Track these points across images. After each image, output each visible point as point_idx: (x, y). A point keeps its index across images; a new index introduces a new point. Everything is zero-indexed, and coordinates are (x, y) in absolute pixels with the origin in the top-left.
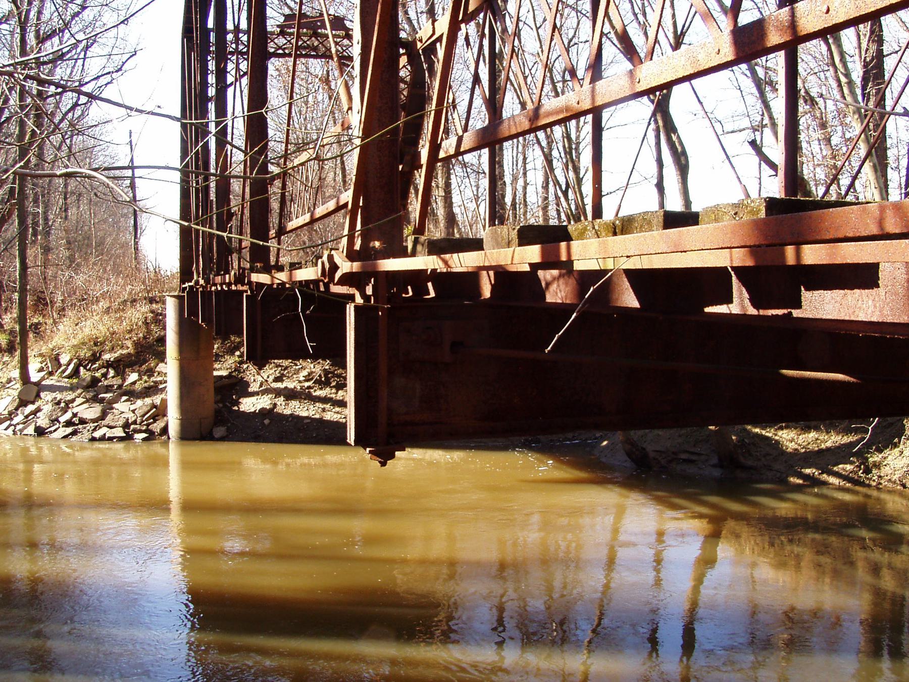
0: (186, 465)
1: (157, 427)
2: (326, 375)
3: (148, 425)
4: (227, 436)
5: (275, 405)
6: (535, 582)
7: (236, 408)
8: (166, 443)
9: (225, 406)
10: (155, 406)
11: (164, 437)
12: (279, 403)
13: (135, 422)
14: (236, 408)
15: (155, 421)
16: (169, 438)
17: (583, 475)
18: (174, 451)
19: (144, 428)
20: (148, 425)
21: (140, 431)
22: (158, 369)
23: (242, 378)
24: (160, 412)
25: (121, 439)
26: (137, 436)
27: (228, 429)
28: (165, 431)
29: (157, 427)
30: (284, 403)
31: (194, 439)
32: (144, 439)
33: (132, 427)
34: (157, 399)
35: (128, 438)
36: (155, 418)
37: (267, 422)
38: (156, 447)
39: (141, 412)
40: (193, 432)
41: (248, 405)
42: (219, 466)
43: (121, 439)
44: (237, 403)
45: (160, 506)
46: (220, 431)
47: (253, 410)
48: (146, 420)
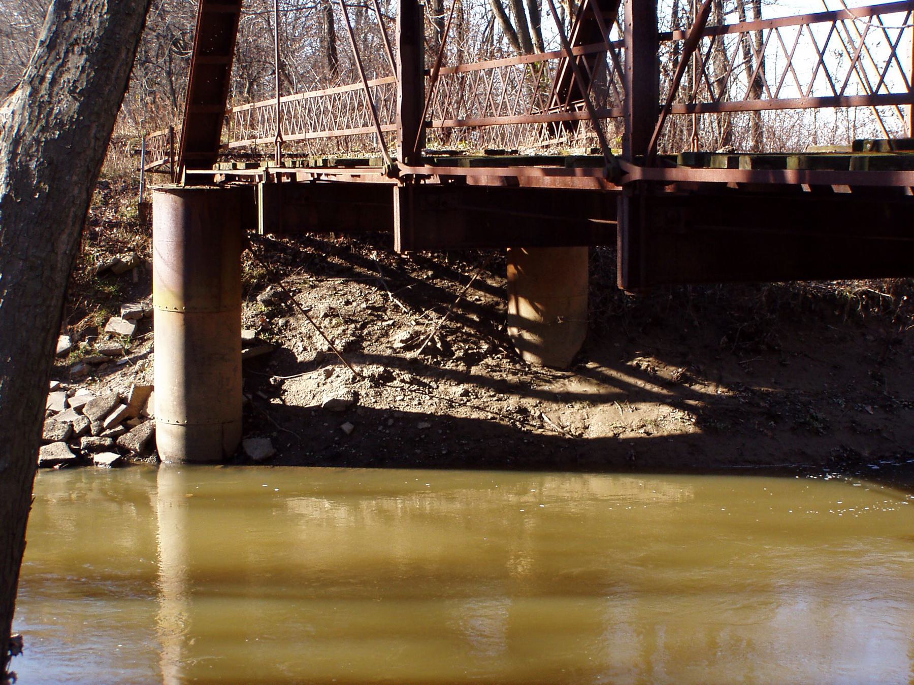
0: (193, 503)
1: (132, 440)
2: (442, 338)
3: (115, 436)
4: (275, 455)
5: (356, 395)
6: (804, 167)
7: (277, 401)
8: (152, 473)
9: (256, 398)
10: (121, 400)
11: (151, 459)
12: (363, 392)
13: (87, 431)
14: (277, 401)
15: (127, 429)
16: (159, 460)
17: (910, 84)
18: (167, 486)
19: (108, 441)
20: (115, 436)
21: (102, 449)
22: (108, 328)
23: (279, 345)
24: (135, 410)
25: (67, 464)
26: (97, 457)
27: (274, 441)
28: (150, 446)
29: (132, 440)
30: (372, 392)
31: (211, 462)
32: (114, 464)
33: (84, 440)
34: (119, 384)
35: (81, 461)
36: (126, 421)
37: (347, 427)
38: (132, 477)
39: (97, 412)
40: (207, 446)
41: (304, 391)
42: (257, 503)
43: (67, 464)
44: (278, 391)
45: (143, 585)
46: (259, 446)
47: (313, 403)
48: (110, 426)
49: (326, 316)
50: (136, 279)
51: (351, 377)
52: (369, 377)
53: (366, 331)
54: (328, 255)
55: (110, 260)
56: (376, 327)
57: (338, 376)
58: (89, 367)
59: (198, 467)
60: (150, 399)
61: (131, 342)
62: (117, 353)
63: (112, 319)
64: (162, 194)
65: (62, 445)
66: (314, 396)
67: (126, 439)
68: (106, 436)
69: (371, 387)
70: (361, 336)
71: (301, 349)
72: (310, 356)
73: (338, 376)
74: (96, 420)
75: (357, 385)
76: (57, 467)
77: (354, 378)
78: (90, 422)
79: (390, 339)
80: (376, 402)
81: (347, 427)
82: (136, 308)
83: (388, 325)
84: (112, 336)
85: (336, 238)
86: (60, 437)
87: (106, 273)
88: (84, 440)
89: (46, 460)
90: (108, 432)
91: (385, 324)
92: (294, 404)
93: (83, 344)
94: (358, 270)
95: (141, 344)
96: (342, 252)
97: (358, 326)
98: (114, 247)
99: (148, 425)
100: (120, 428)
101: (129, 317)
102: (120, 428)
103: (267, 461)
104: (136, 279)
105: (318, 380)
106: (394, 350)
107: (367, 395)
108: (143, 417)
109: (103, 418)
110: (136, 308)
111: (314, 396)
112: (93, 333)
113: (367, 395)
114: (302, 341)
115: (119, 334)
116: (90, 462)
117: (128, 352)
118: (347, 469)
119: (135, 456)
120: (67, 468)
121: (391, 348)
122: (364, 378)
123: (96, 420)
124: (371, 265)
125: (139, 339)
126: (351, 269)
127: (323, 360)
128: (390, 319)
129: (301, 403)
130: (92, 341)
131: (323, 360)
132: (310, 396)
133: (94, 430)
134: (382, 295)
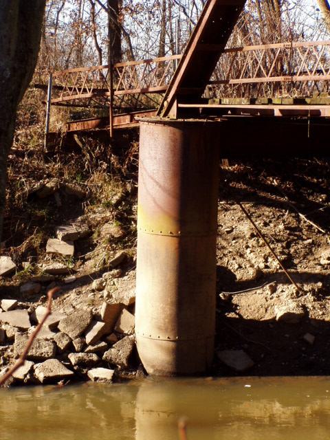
1: (118, 353)
3: (99, 352)
5: (304, 307)
12: (309, 306)
14: (232, 315)
15: (110, 346)
29: (118, 353)
46: (237, 358)
47: (268, 317)
49: (252, 236)
50: (59, 203)
51: (295, 292)
52: (310, 291)
53: (292, 250)
54: (230, 181)
55: (37, 185)
56: (299, 246)
57: (282, 291)
58: (39, 285)
59: (194, 380)
60: (122, 316)
61: (74, 262)
62: (65, 272)
63: (50, 241)
64: (152, 126)
65: (55, 362)
66: (266, 310)
67: (110, 354)
68: (90, 351)
69: (314, 300)
70: (289, 254)
71: (237, 266)
72: (250, 273)
73: (282, 291)
74: (76, 337)
75: (302, 299)
76: (60, 383)
77: (297, 293)
78: (71, 340)
79: (316, 257)
80: (323, 314)
81: (309, 338)
82: (72, 229)
83: (309, 244)
84: (55, 256)
85: (230, 165)
86: (50, 355)
87: (34, 196)
88: (73, 358)
89: (49, 377)
90: (90, 348)
91: (306, 242)
92: (251, 317)
93: (26, 265)
94: (262, 194)
95: (83, 263)
96: (239, 177)
97: (284, 244)
98: (36, 174)
99: (128, 341)
100: (103, 344)
101: (67, 239)
102: (103, 344)
103: (248, 372)
104: (59, 203)
105: (264, 295)
106: (323, 266)
107: (314, 308)
108: (121, 335)
109: (82, 335)
110: (72, 229)
111: (266, 310)
112: (35, 254)
113: (314, 308)
114: (234, 259)
115: (61, 255)
116: (86, 378)
117: (74, 272)
118: (299, 377)
119: (122, 370)
120: (69, 384)
121: (320, 265)
122: (306, 293)
123: (76, 337)
124: (272, 190)
125: (81, 259)
126: (255, 193)
127: (261, 279)
128: (308, 238)
129: (256, 316)
130: (35, 261)
131: (261, 279)
132: (263, 310)
133: (77, 346)
134: (293, 217)
